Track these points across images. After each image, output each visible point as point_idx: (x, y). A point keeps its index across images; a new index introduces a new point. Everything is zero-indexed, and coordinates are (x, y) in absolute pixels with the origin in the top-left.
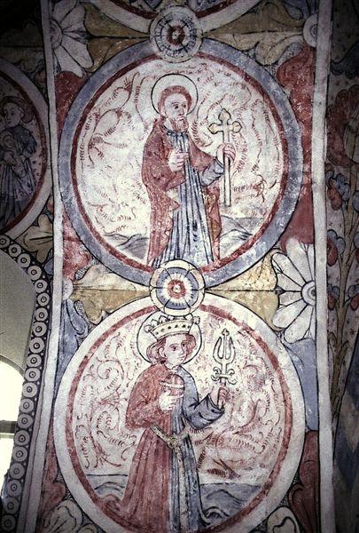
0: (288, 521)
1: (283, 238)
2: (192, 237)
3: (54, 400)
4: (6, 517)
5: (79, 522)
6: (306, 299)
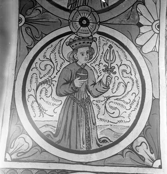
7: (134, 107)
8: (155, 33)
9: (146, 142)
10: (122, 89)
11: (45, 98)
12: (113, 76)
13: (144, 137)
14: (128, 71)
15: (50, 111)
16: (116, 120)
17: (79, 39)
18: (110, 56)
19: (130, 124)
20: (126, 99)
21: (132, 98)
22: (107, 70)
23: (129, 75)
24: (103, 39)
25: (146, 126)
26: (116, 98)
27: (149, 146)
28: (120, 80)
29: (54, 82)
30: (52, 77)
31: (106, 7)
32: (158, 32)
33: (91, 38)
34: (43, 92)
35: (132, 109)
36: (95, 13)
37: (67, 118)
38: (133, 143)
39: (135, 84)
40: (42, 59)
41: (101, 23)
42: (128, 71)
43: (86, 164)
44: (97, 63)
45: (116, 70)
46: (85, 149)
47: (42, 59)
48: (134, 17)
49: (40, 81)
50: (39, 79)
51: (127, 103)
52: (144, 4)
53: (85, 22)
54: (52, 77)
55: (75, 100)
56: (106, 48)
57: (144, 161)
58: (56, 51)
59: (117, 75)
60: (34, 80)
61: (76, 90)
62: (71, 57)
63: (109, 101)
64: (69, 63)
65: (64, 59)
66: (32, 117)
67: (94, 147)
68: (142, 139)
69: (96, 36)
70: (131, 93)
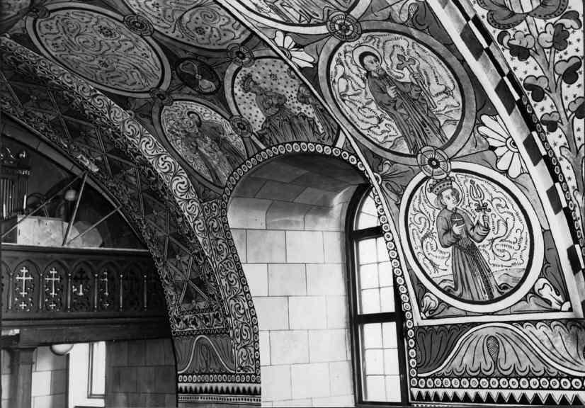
0: (546, 286)
1: (478, 117)
2: (426, 132)
3: (400, 241)
4: (407, 313)
5: (437, 302)
6: (513, 149)
7: (523, 244)
8: (514, 152)
9: (549, 283)
10: (503, 228)
11: (432, 252)
12: (489, 214)
13: (545, 278)
14: (504, 205)
15: (442, 266)
16: (509, 263)
17: (437, 182)
18: (477, 193)
19: (525, 266)
20: (512, 238)
21: (518, 235)
22: (479, 209)
23: (506, 209)
24: (461, 176)
25: (543, 265)
26: (500, 239)
27: (553, 287)
28: (498, 218)
29: (434, 234)
30: (431, 229)
31: (446, 141)
32: (517, 150)
33: (448, 178)
34: (429, 247)
35: (522, 248)
36: (439, 151)
37: (460, 269)
38: (534, 286)
39: (516, 217)
40: (414, 213)
41: (451, 159)
42: (504, 205)
43: (493, 314)
44: (467, 204)
45: (489, 206)
46: (487, 299)
47: (414, 213)
48: (481, 142)
49: (422, 235)
50: (420, 234)
51: (514, 243)
52: (484, 125)
53: (434, 163)
54: (431, 229)
55: (460, 247)
56: (468, 184)
57: (551, 304)
58: (423, 201)
59: (493, 211)
60: (416, 237)
61: (458, 238)
62: (439, 203)
63: (494, 244)
64: (439, 211)
65: (432, 207)
66: (428, 274)
67: (496, 295)
68: (543, 281)
69: (452, 174)
70: (514, 231)
